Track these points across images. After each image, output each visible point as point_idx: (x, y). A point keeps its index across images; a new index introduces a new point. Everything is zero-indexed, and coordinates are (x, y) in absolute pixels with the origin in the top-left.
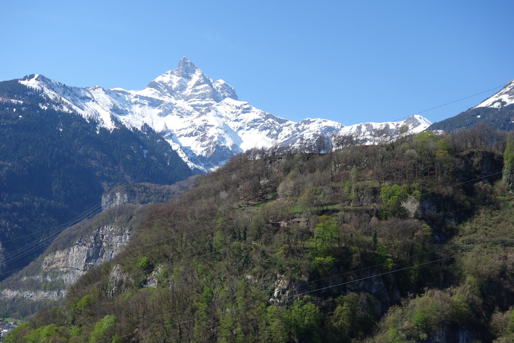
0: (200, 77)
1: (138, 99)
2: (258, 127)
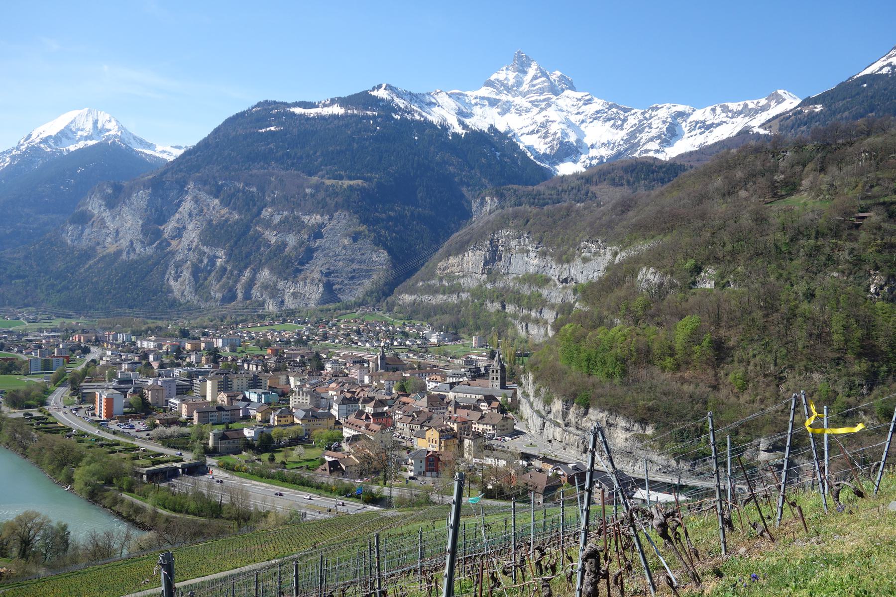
0: (536, 70)
1: (478, 100)
2: (602, 118)
